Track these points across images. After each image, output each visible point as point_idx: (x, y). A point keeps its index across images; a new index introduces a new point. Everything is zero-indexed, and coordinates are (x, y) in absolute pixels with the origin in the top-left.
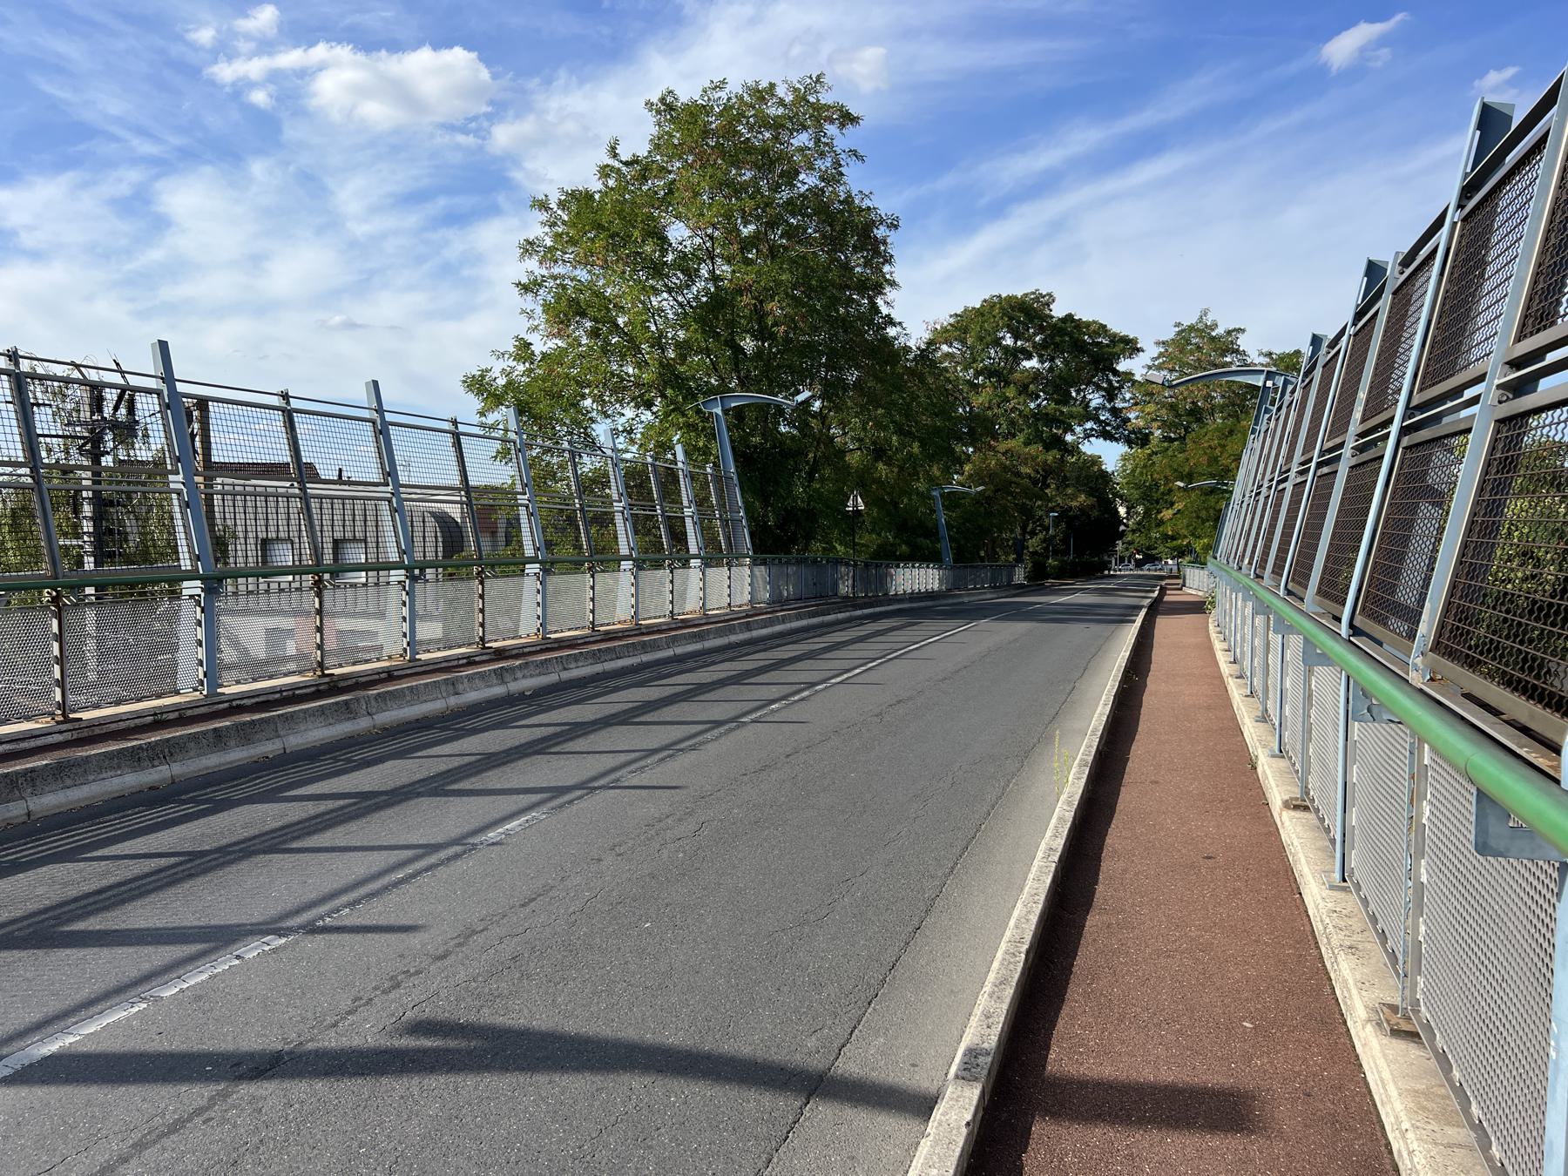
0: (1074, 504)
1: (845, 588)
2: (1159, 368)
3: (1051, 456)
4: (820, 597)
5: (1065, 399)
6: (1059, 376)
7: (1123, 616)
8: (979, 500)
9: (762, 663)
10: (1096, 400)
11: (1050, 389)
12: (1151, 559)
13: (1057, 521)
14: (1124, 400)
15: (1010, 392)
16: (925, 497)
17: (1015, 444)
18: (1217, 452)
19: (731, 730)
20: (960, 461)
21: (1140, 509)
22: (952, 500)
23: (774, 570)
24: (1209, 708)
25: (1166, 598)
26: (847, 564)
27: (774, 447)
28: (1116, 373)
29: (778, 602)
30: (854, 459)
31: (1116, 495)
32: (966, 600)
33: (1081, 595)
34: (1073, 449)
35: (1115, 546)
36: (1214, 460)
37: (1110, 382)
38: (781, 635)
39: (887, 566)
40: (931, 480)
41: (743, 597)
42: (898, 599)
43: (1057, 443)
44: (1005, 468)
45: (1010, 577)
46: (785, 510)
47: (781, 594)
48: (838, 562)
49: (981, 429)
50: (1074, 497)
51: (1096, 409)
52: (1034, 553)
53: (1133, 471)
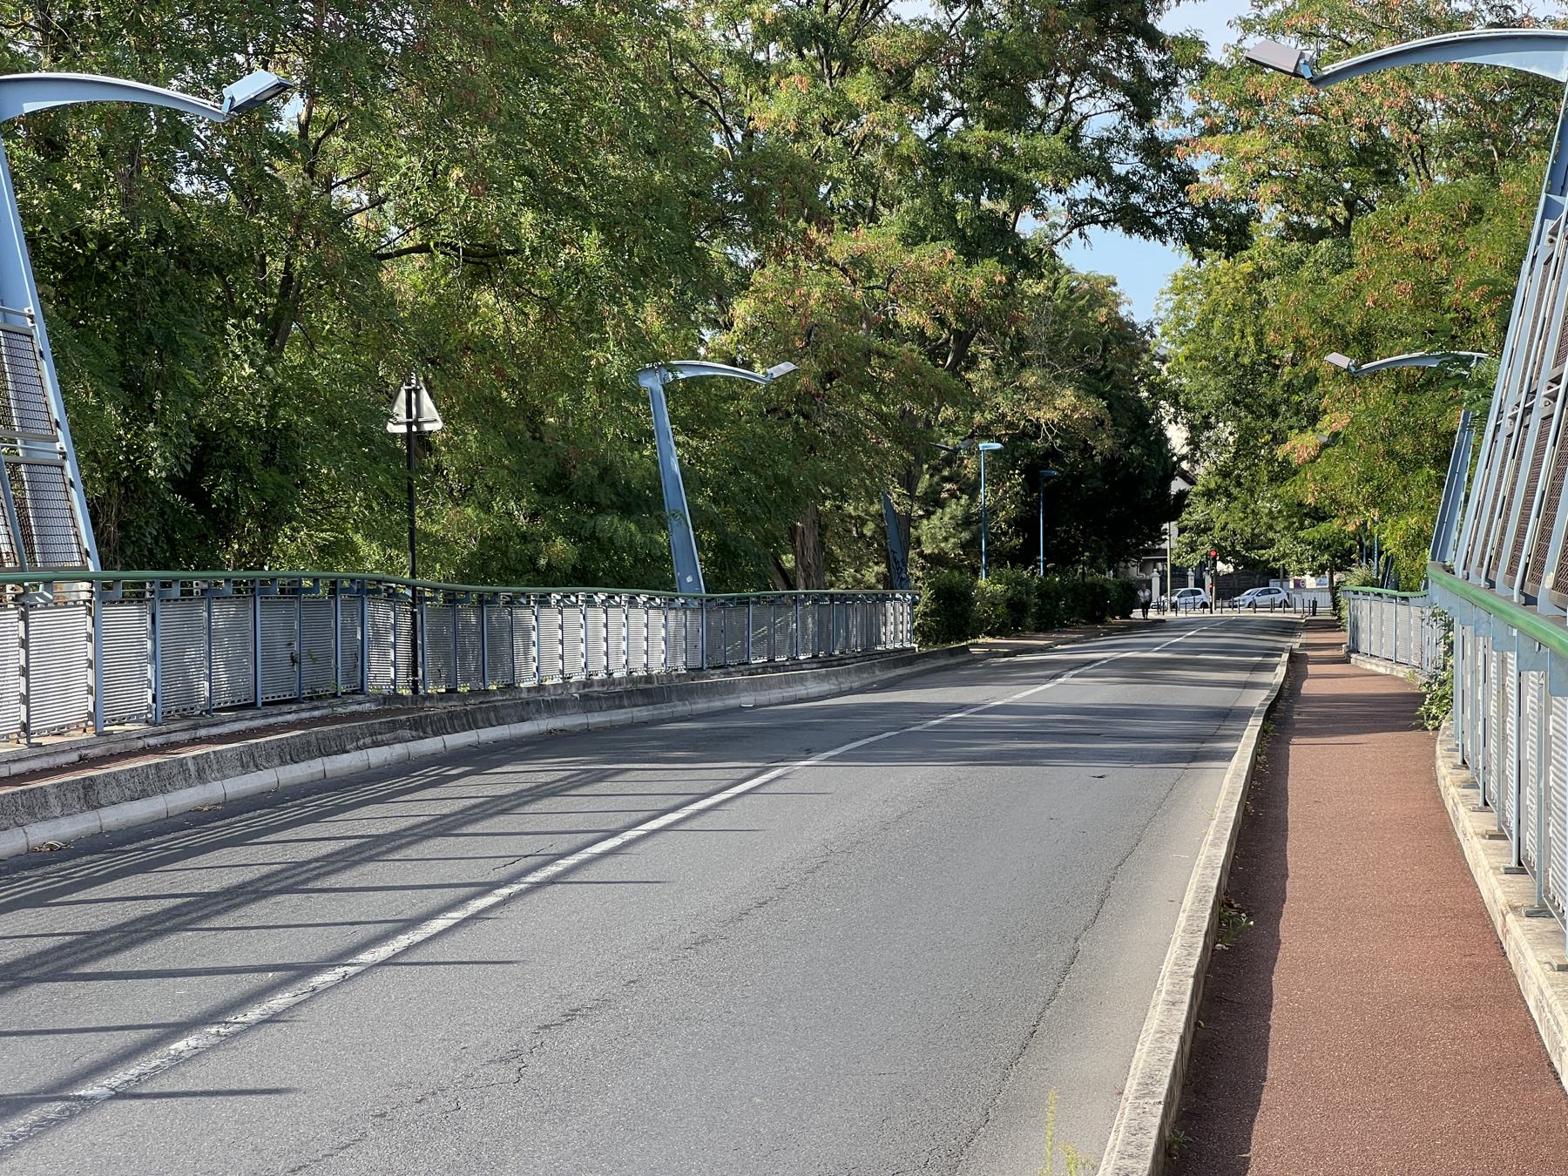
0: (1046, 415)
1: (386, 671)
2: (1274, 28)
3: (983, 276)
4: (309, 700)
5: (1016, 115)
6: (999, 49)
7: (1199, 739)
8: (783, 405)
9: (137, 910)
10: (1100, 116)
11: (970, 82)
12: (1257, 573)
13: (1000, 464)
14: (1177, 116)
15: (860, 88)
16: (625, 393)
17: (877, 240)
18: (1440, 268)
19: (47, 1125)
20: (725, 287)
21: (1226, 431)
22: (699, 406)
23: (170, 615)
24: (1457, 1005)
25: (1309, 688)
26: (392, 596)
27: (159, 238)
28: (1154, 39)
29: (182, 716)
30: (407, 279)
31: (1157, 390)
32: (747, 700)
33: (1071, 679)
34: (1031, 261)
35: (1158, 536)
36: (1429, 295)
37: (1137, 66)
38: (197, 818)
39: (511, 602)
40: (637, 342)
41: (67, 706)
42: (543, 701)
43: (990, 239)
44: (850, 312)
45: (871, 633)
46: (202, 433)
47: (190, 691)
48: (366, 590)
49: (776, 195)
50: (1043, 396)
51: (1103, 143)
52: (937, 560)
53: (1206, 322)
